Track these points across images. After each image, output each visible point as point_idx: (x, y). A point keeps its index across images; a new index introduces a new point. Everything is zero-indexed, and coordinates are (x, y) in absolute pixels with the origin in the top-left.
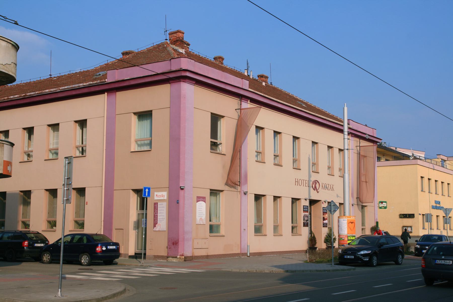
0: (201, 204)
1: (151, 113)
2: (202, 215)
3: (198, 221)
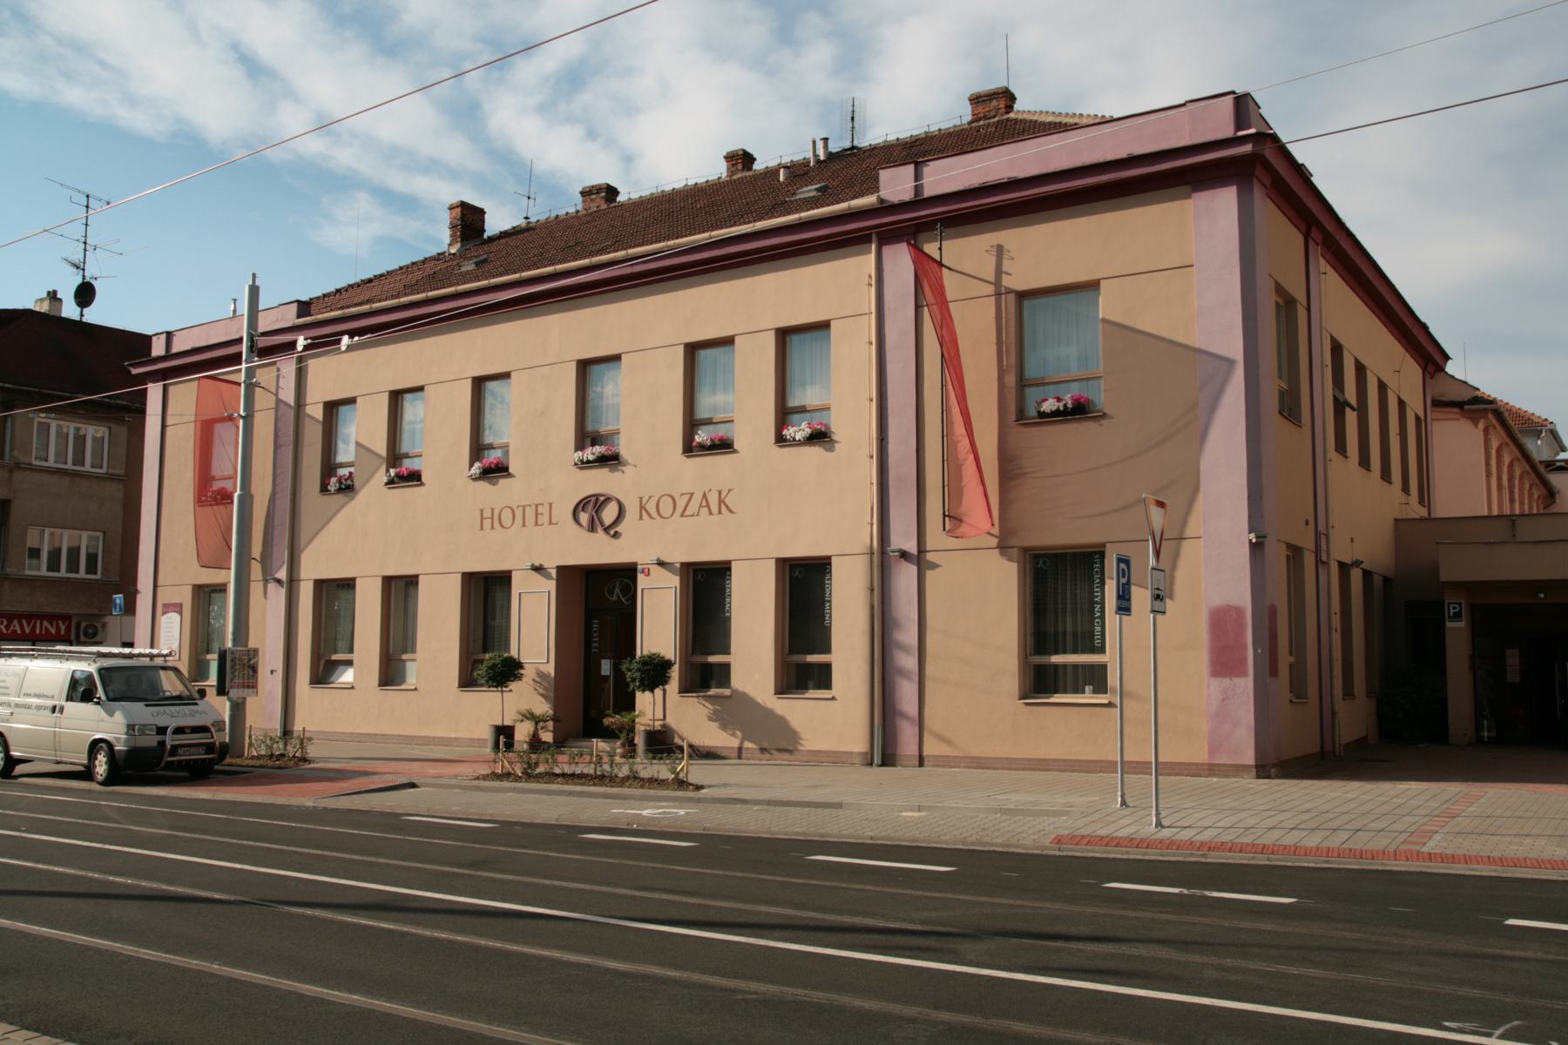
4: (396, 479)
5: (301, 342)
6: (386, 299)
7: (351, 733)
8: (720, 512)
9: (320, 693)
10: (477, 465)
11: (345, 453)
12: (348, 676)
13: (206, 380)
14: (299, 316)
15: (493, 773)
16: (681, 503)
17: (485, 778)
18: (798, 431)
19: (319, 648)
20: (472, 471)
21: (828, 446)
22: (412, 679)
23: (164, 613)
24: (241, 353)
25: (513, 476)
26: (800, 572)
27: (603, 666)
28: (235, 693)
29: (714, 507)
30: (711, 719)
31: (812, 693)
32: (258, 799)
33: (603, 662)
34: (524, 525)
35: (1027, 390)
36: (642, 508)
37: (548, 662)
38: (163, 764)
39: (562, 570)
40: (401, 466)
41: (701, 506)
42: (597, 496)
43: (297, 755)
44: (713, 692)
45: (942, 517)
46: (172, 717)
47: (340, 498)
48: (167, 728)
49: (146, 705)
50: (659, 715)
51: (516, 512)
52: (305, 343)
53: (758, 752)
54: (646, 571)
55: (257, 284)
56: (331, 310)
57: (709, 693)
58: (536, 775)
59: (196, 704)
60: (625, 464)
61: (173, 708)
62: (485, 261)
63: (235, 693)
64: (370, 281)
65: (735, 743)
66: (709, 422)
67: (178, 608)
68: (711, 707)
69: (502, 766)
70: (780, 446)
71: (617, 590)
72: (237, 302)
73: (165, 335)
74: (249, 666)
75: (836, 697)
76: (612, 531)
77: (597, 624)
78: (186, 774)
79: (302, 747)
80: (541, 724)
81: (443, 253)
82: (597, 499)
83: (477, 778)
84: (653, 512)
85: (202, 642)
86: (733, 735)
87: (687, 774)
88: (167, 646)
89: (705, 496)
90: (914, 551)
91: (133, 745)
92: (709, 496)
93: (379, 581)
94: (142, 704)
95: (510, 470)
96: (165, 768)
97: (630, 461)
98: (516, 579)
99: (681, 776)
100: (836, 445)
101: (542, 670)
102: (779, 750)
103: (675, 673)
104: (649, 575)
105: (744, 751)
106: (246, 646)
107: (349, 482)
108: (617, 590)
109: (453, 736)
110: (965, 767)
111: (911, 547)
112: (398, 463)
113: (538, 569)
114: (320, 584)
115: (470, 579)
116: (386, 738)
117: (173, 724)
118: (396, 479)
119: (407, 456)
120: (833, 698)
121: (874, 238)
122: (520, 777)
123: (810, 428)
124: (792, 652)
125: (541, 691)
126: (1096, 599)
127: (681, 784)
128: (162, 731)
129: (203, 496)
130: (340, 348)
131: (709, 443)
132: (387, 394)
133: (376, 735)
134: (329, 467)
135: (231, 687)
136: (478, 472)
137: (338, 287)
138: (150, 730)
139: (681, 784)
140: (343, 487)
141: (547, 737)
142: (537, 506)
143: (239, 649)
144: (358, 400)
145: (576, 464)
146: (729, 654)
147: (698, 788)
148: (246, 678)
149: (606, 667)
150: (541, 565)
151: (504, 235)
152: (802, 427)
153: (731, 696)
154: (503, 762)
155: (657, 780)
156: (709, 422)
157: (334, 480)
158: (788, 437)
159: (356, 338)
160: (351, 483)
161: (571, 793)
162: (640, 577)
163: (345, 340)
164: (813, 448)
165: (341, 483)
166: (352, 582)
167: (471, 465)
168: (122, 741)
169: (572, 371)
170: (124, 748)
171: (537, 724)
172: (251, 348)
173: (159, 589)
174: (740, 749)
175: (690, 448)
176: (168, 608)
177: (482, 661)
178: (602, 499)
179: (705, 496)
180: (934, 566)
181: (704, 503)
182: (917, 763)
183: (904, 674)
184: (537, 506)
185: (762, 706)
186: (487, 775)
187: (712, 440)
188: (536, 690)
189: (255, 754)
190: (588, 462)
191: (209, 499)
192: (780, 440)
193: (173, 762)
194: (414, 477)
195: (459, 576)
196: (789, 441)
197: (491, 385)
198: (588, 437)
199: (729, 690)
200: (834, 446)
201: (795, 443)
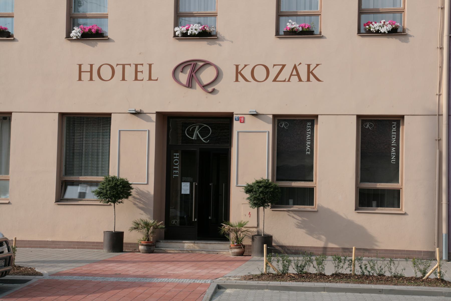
8: (308, 80)
16: (274, 72)
17: (260, 277)
21: (403, 38)
27: (183, 187)
29: (304, 76)
30: (299, 227)
33: (183, 184)
34: (123, 79)
35: (282, 19)
36: (238, 73)
41: (291, 75)
42: (195, 62)
60: (223, 39)
75: (407, 213)
84: (249, 77)
86: (319, 238)
89: (295, 67)
100: (410, 38)
101: (142, 189)
108: (197, 132)
122: (293, 277)
124: (363, 180)
126: (394, 148)
131: (300, 29)
146: (312, 181)
149: (186, 188)
161: (380, 291)
166: (9, 115)
178: (201, 64)
179: (295, 67)
181: (295, 73)
184: (136, 65)
188: (135, 204)
192: (68, 36)
200: (409, 39)
201: (72, 40)
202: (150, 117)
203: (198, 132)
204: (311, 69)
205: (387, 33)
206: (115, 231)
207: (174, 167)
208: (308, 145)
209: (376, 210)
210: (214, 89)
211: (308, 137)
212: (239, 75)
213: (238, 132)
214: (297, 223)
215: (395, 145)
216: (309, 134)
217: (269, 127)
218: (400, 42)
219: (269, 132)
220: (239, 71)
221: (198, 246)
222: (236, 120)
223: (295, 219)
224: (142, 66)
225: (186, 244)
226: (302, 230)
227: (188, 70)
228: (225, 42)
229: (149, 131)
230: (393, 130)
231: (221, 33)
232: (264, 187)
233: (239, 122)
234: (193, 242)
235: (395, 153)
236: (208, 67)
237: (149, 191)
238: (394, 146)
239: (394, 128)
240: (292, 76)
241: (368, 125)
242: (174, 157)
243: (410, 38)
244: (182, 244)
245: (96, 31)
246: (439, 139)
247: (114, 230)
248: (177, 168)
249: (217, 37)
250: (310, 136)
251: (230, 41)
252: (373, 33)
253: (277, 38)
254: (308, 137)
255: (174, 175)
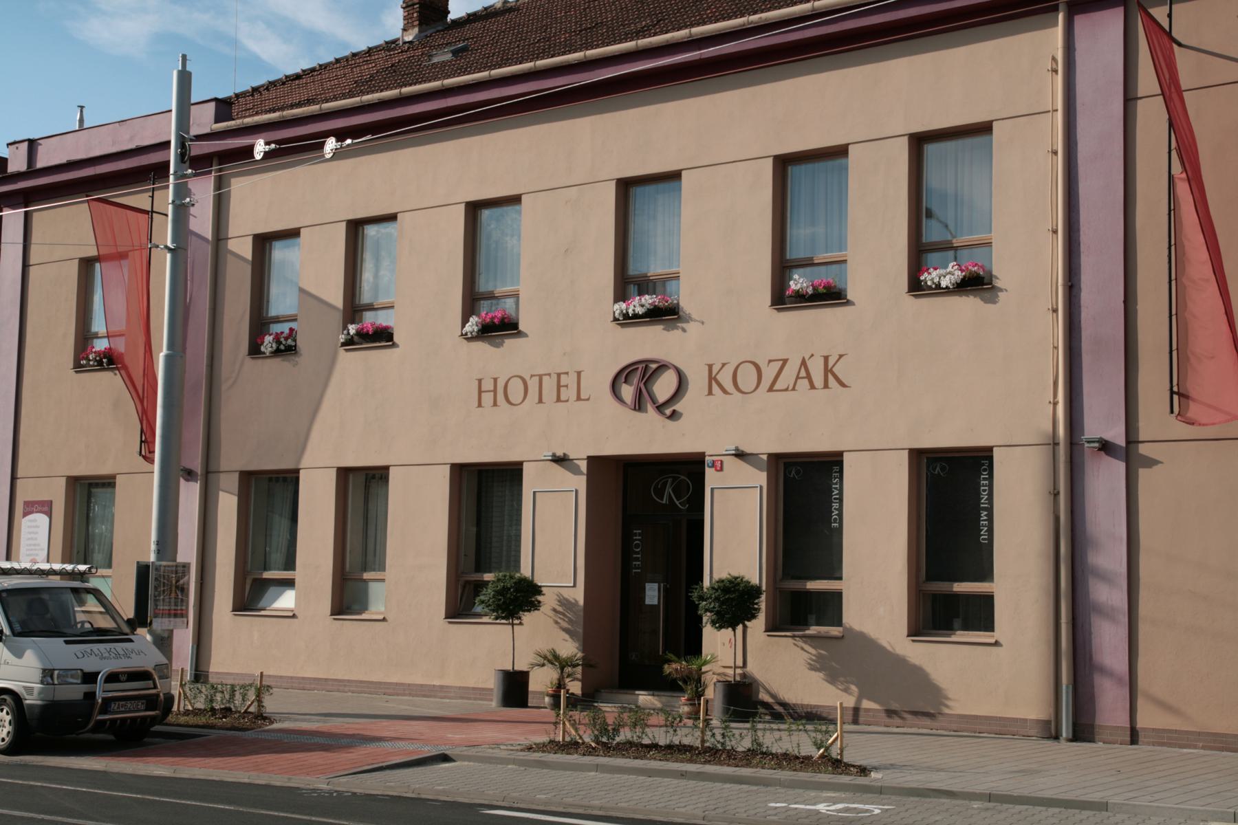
0: (35, 521)
1: (295, 475)
2: (35, 550)
3: (656, 586)
4: (356, 339)
5: (260, 148)
6: (335, 98)
7: (292, 678)
8: (826, 386)
9: (246, 622)
10: (474, 320)
11: (281, 302)
12: (287, 600)
13: (95, 203)
14: (218, 120)
15: (551, 742)
16: (769, 373)
17: (542, 748)
18: (948, 275)
19: (245, 562)
20: (468, 328)
21: (987, 295)
22: (377, 607)
23: (25, 514)
24: (168, 163)
25: (526, 335)
26: (798, 473)
27: (648, 593)
28: (159, 624)
29: (818, 380)
30: (812, 668)
31: (960, 636)
32: (243, 777)
33: (648, 586)
34: (540, 401)
36: (712, 379)
37: (575, 586)
38: (90, 725)
39: (596, 463)
40: (361, 321)
41: (798, 377)
42: (647, 362)
43: (250, 710)
44: (813, 630)
45: (1168, 393)
46: (101, 658)
47: (277, 363)
48: (98, 673)
49: (67, 642)
50: (740, 662)
51: (529, 383)
52: (267, 148)
53: (884, 715)
54: (718, 464)
55: (188, 68)
56: (257, 113)
57: (807, 632)
58: (618, 744)
59: (130, 641)
60: (688, 319)
61: (102, 646)
62: (464, 49)
63: (159, 624)
64: (297, 77)
65: (850, 702)
66: (807, 263)
67: (46, 507)
68: (813, 651)
69: (564, 731)
70: (915, 296)
71: (669, 490)
72: (84, 110)
73: (26, 144)
74: (177, 587)
75: (1001, 641)
76: (668, 410)
77: (640, 535)
78: (111, 737)
79: (259, 699)
80: (568, 670)
81: (394, 42)
82: (646, 366)
83: (530, 748)
84: (729, 385)
85: (78, 552)
86: (846, 690)
87: (842, 750)
88: (29, 558)
89: (804, 363)
90: (1121, 441)
91: (51, 698)
92: (809, 363)
93: (333, 473)
94: (59, 641)
95: (521, 327)
96: (94, 730)
97: (694, 316)
98: (528, 473)
99: (835, 753)
101: (566, 596)
102: (915, 713)
103: (762, 602)
104: (721, 470)
105: (862, 713)
106: (175, 560)
107: (290, 342)
109: (437, 682)
110: (1203, 748)
111: (1117, 435)
112: (357, 318)
113: (560, 460)
114: (248, 479)
115: (460, 472)
116: (443, 691)
117: (106, 668)
118: (356, 339)
119: (370, 308)
120: (997, 644)
121: (1061, 7)
122: (593, 748)
123: (962, 271)
124: (931, 577)
125: (565, 625)
126: (986, 513)
127: (837, 765)
128: (90, 678)
129: (83, 358)
130: (323, 156)
131: (810, 291)
132: (344, 224)
133: (326, 680)
134: (260, 322)
135: (156, 616)
136: (476, 329)
137: (255, 84)
138: (72, 677)
139: (837, 765)
140: (282, 347)
141: (575, 687)
142: (559, 375)
143: (164, 563)
144: (524, 198)
145: (615, 319)
146: (841, 578)
147: (863, 771)
148: (173, 604)
149: (652, 594)
150: (565, 454)
151: (472, 18)
152: (950, 269)
153: (843, 636)
154: (564, 723)
155: (797, 758)
156: (807, 263)
157: (268, 339)
158: (929, 283)
159: (349, 141)
160: (293, 344)
161: (683, 775)
162: (709, 473)
163: (331, 144)
164: (964, 298)
165: (278, 342)
166: (295, 475)
167: (465, 321)
168: (36, 692)
169: (459, 213)
170: (39, 702)
171: (562, 669)
172: (182, 157)
173: (19, 483)
174: (856, 710)
175: (782, 298)
176: (32, 507)
177: (485, 584)
178: (654, 366)
179: (804, 363)
180: (1150, 463)
181: (803, 373)
182: (1128, 739)
183: (1107, 613)
184: (559, 375)
185: (889, 652)
186: (544, 745)
187: (814, 288)
188: (557, 622)
189: (190, 708)
190: (636, 316)
191: (91, 363)
192: (916, 286)
193: (104, 721)
194: (383, 336)
195: (447, 469)
196: (930, 288)
197: (371, 231)
198: (631, 283)
199: (840, 629)
200: (998, 296)
202: (578, 467)
203: (670, 490)
204: (830, 364)
205: (621, 319)
206: (515, 669)
207: (635, 556)
208: (835, 509)
209: (953, 636)
210: (674, 411)
211: (835, 495)
212: (713, 383)
213: (712, 489)
214: (809, 661)
215: (986, 505)
216: (836, 488)
217: (761, 478)
218: (982, 302)
219: (761, 487)
220: (713, 376)
221: (660, 701)
222: (709, 466)
223: (805, 653)
224: (566, 375)
225: (641, 697)
226: (818, 673)
227: (635, 379)
228: (692, 323)
229: (577, 491)
230: (982, 476)
231: (685, 309)
232: (722, 590)
233: (714, 469)
234: (651, 693)
235: (987, 522)
236: (664, 372)
237: (578, 599)
238: (985, 509)
239: (985, 471)
240: (799, 381)
241: (938, 469)
242: (635, 538)
243: (1000, 294)
244: (633, 697)
245: (501, 322)
246: (1056, 491)
247: (513, 668)
248: (639, 558)
249: (845, 301)
250: (837, 492)
251: (699, 321)
252: (932, 289)
253: (911, 297)
254: (835, 495)
255: (634, 571)
